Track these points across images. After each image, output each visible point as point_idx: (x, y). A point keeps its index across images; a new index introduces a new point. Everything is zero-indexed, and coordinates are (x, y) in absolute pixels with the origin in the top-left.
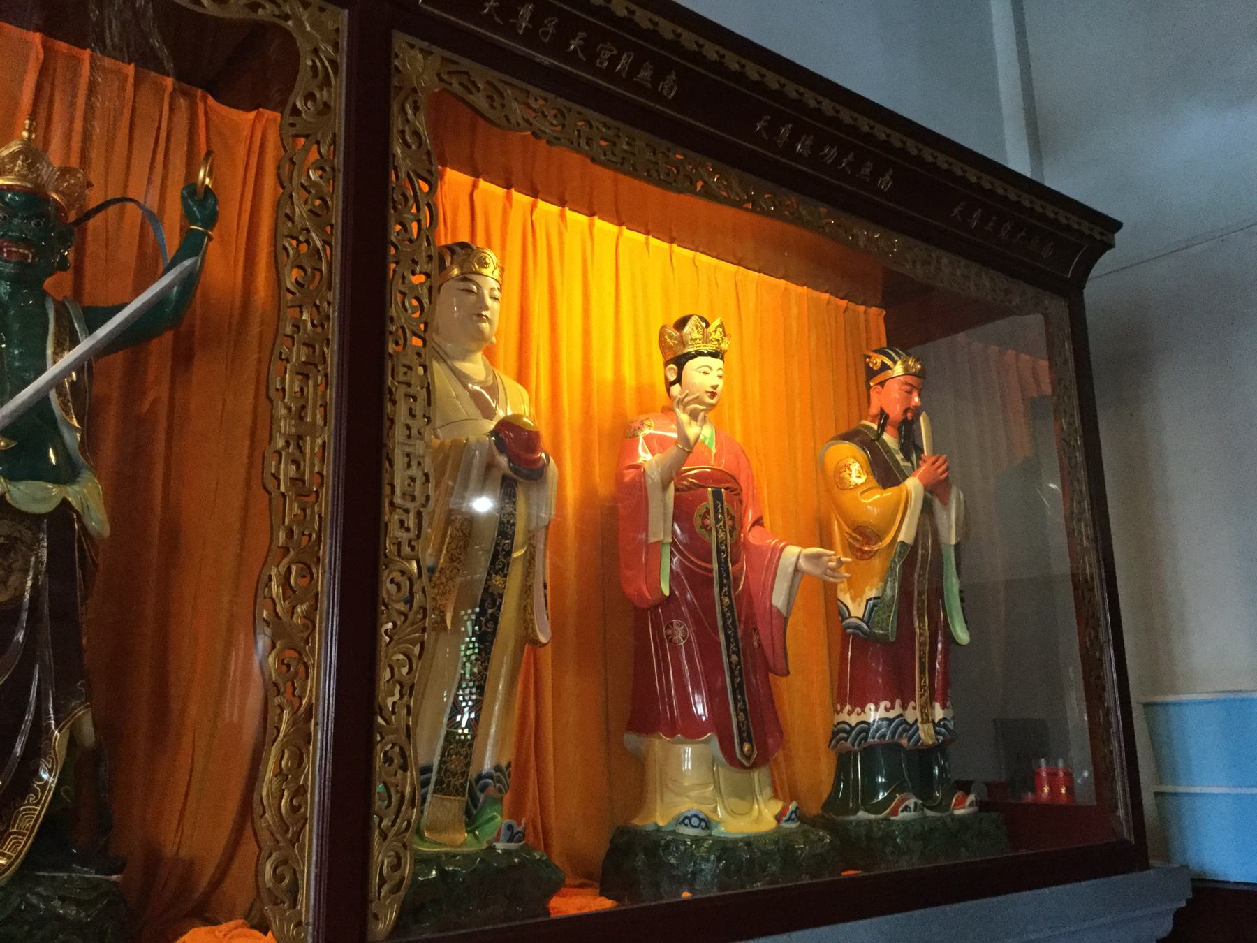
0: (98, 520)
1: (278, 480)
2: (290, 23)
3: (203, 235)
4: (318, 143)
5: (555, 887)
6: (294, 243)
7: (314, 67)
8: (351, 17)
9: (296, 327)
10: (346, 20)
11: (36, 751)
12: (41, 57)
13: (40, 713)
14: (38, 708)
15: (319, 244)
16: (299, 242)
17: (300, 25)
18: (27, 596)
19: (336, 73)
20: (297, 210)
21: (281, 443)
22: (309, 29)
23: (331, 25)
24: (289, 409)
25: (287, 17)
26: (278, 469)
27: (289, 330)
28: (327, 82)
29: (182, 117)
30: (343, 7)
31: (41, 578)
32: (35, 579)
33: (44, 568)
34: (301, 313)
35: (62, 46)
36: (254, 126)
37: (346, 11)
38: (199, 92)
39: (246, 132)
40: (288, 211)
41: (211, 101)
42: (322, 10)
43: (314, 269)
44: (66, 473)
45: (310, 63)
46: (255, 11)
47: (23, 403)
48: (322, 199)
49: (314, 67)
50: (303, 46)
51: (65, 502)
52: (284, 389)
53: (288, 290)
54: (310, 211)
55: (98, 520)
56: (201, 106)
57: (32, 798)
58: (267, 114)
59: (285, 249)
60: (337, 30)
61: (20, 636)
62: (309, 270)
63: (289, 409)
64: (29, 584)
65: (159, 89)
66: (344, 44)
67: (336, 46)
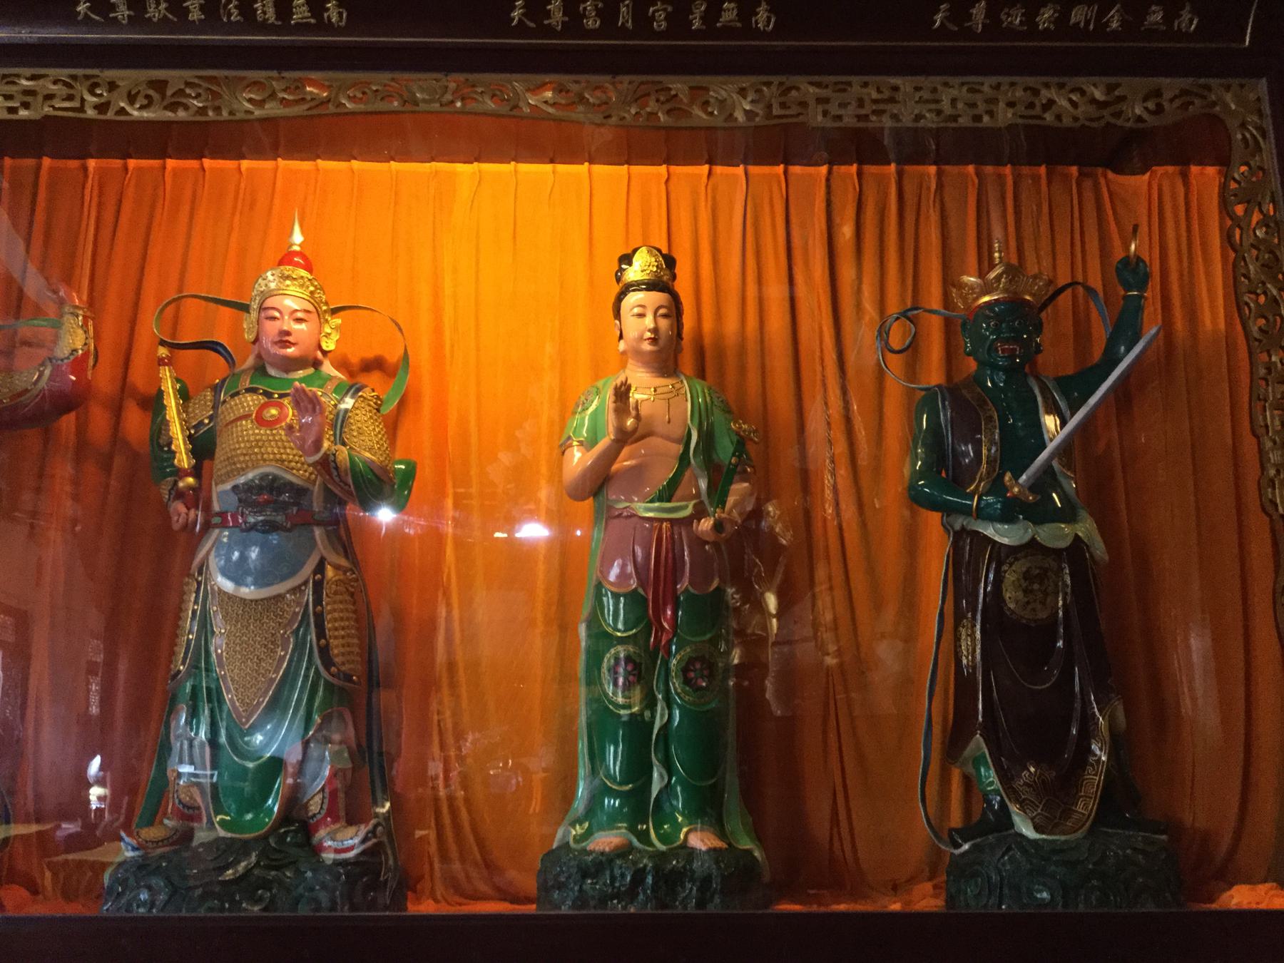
0: (1099, 548)
1: (1276, 505)
2: (1218, 108)
3: (1140, 297)
4: (1260, 205)
5: (1229, 876)
6: (1253, 296)
7: (1244, 137)
8: (1269, 83)
9: (1269, 370)
10: (1265, 88)
11: (1088, 732)
12: (976, 181)
13: (1086, 703)
14: (1083, 699)
15: (1275, 292)
16: (1258, 295)
17: (1226, 106)
18: (1061, 613)
19: (1264, 136)
20: (1251, 267)
21: (1272, 472)
22: (1233, 107)
23: (1252, 96)
24: (1275, 443)
25: (1214, 104)
26: (1274, 494)
27: (1262, 372)
28: (1258, 148)
29: (1089, 195)
30: (1260, 76)
31: (1069, 599)
32: (1064, 600)
33: (1069, 590)
34: (1270, 357)
35: (989, 169)
36: (1149, 184)
37: (1264, 80)
38: (1100, 170)
39: (1145, 187)
40: (1243, 271)
41: (1111, 175)
42: (1242, 86)
43: (1274, 315)
44: (1068, 514)
45: (1239, 136)
46: (1187, 109)
47: (1038, 470)
48: (1271, 252)
49: (1244, 137)
50: (1233, 124)
51: (1077, 537)
52: (1267, 426)
53: (1256, 340)
54: (1263, 265)
55: (1099, 548)
56: (1102, 181)
57: (1090, 769)
58: (1160, 170)
59: (1247, 304)
60: (1259, 99)
61: (1060, 644)
62: (1271, 318)
63: (1275, 443)
64: (1061, 603)
65: (1067, 177)
66: (1267, 110)
67: (1260, 114)
